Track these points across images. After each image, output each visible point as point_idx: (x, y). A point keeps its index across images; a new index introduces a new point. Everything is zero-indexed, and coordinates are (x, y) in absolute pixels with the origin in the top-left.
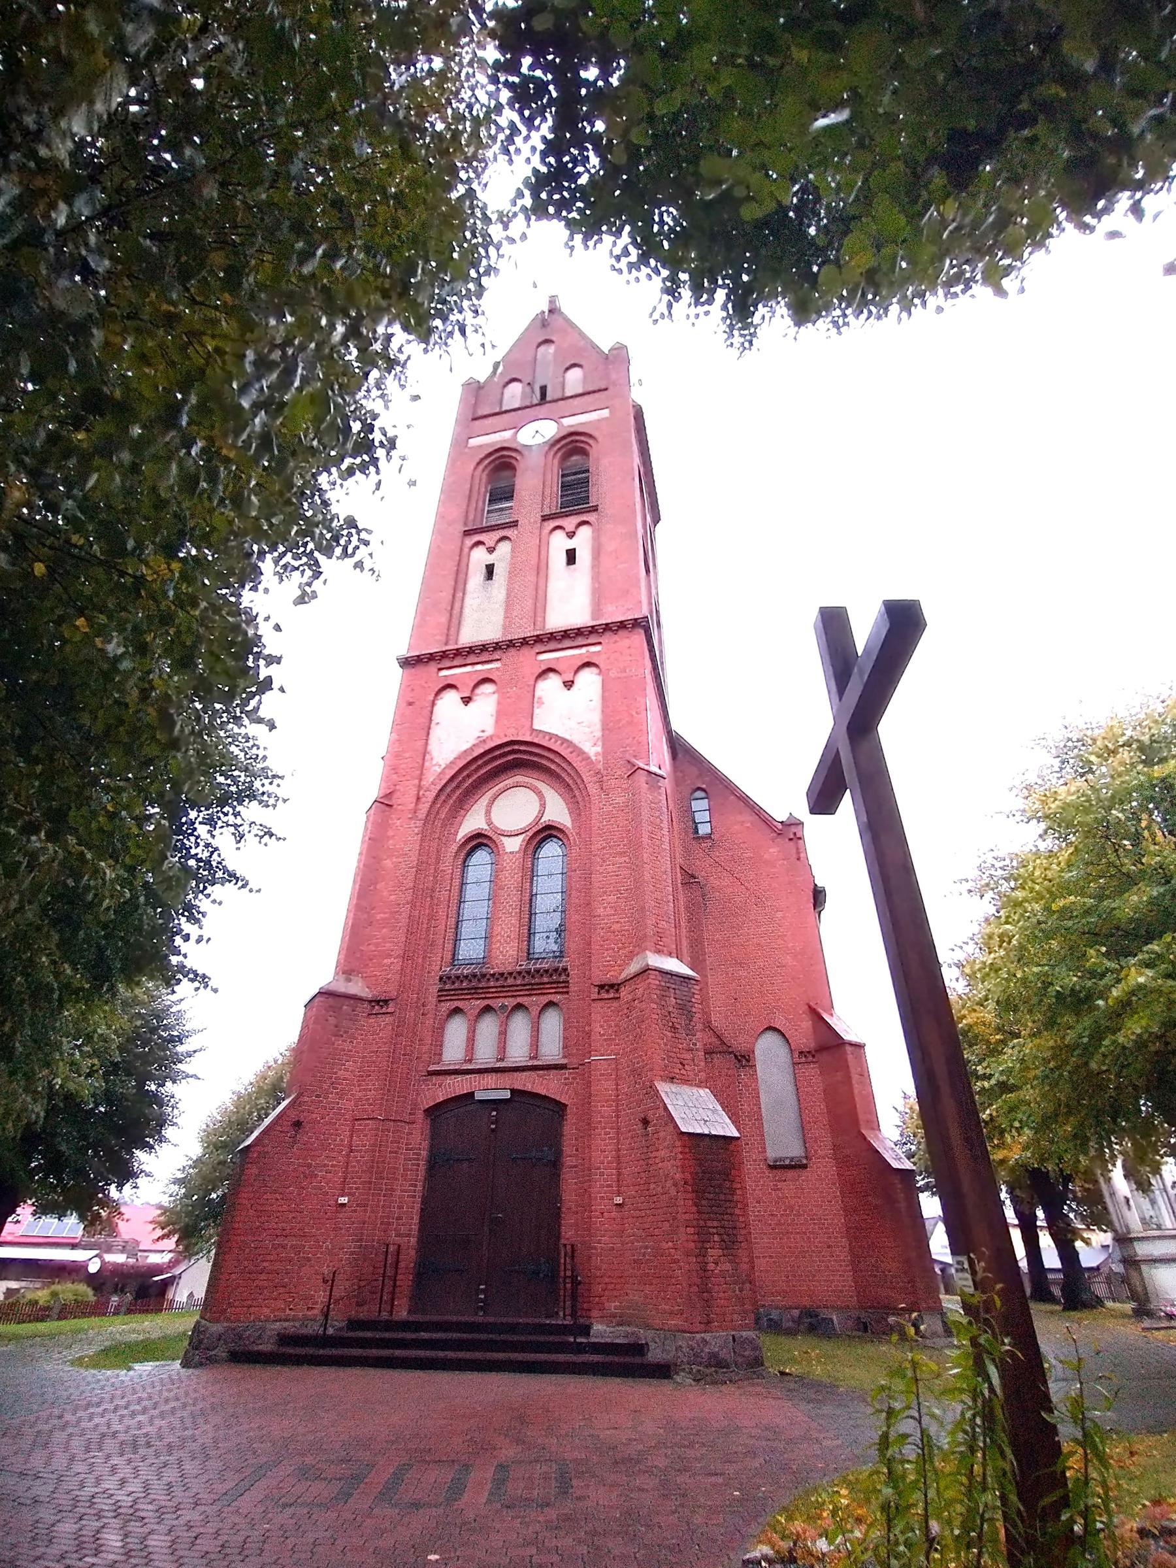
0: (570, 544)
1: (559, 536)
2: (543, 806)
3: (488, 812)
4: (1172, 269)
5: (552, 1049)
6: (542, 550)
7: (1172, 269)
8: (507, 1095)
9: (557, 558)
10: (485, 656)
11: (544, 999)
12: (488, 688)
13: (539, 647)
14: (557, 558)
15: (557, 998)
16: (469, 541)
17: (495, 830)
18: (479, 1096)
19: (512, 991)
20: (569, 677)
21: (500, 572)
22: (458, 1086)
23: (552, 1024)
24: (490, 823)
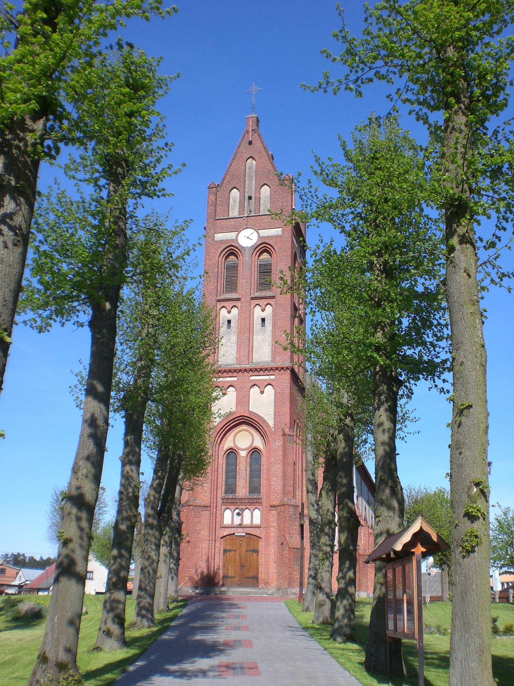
0: (263, 315)
1: (258, 309)
2: (253, 440)
3: (234, 440)
4: (2, 435)
5: (257, 521)
6: (251, 315)
7: (2, 435)
8: (244, 534)
9: (257, 322)
10: (230, 374)
11: (232, 305)
12: (231, 389)
13: (251, 373)
14: (257, 322)
15: (258, 507)
16: (219, 305)
17: (237, 447)
18: (236, 534)
19: (245, 504)
20: (262, 389)
21: (269, 323)
22: (231, 531)
23: (257, 513)
24: (235, 445)
